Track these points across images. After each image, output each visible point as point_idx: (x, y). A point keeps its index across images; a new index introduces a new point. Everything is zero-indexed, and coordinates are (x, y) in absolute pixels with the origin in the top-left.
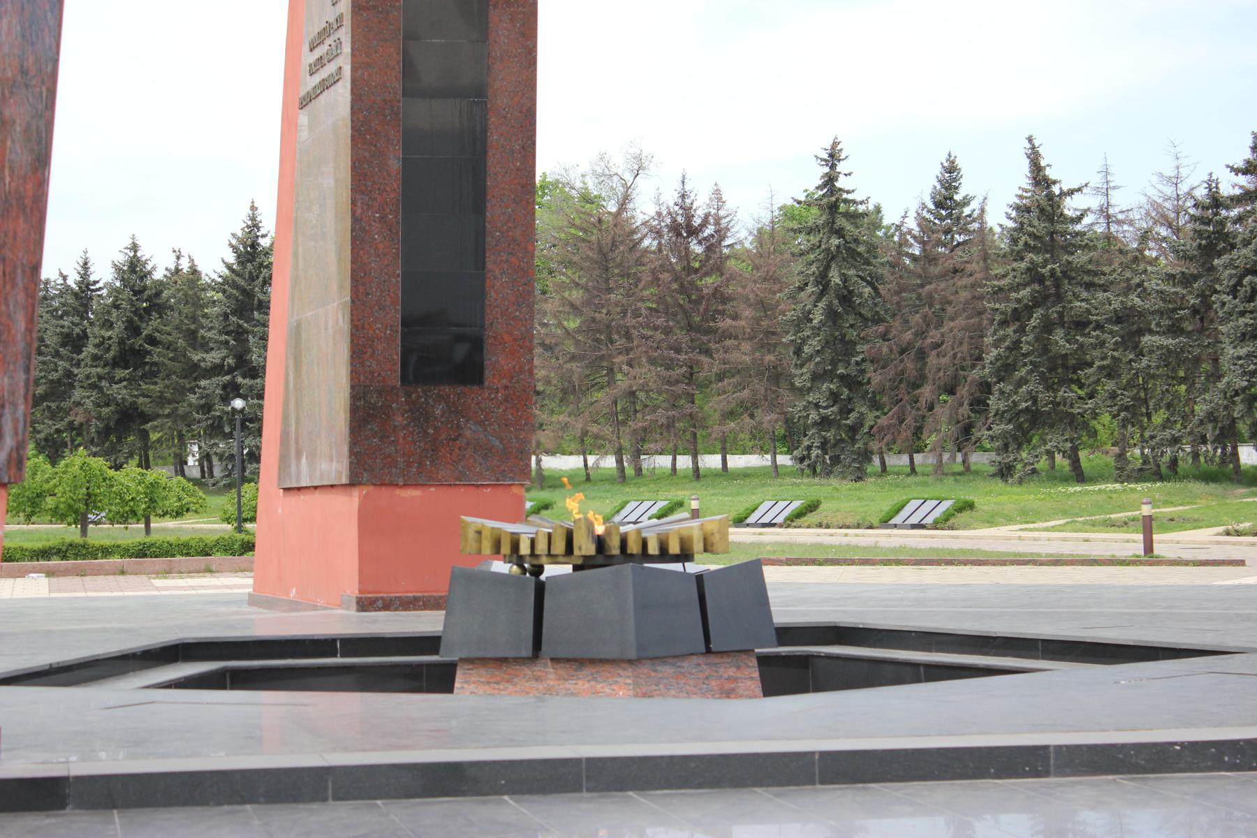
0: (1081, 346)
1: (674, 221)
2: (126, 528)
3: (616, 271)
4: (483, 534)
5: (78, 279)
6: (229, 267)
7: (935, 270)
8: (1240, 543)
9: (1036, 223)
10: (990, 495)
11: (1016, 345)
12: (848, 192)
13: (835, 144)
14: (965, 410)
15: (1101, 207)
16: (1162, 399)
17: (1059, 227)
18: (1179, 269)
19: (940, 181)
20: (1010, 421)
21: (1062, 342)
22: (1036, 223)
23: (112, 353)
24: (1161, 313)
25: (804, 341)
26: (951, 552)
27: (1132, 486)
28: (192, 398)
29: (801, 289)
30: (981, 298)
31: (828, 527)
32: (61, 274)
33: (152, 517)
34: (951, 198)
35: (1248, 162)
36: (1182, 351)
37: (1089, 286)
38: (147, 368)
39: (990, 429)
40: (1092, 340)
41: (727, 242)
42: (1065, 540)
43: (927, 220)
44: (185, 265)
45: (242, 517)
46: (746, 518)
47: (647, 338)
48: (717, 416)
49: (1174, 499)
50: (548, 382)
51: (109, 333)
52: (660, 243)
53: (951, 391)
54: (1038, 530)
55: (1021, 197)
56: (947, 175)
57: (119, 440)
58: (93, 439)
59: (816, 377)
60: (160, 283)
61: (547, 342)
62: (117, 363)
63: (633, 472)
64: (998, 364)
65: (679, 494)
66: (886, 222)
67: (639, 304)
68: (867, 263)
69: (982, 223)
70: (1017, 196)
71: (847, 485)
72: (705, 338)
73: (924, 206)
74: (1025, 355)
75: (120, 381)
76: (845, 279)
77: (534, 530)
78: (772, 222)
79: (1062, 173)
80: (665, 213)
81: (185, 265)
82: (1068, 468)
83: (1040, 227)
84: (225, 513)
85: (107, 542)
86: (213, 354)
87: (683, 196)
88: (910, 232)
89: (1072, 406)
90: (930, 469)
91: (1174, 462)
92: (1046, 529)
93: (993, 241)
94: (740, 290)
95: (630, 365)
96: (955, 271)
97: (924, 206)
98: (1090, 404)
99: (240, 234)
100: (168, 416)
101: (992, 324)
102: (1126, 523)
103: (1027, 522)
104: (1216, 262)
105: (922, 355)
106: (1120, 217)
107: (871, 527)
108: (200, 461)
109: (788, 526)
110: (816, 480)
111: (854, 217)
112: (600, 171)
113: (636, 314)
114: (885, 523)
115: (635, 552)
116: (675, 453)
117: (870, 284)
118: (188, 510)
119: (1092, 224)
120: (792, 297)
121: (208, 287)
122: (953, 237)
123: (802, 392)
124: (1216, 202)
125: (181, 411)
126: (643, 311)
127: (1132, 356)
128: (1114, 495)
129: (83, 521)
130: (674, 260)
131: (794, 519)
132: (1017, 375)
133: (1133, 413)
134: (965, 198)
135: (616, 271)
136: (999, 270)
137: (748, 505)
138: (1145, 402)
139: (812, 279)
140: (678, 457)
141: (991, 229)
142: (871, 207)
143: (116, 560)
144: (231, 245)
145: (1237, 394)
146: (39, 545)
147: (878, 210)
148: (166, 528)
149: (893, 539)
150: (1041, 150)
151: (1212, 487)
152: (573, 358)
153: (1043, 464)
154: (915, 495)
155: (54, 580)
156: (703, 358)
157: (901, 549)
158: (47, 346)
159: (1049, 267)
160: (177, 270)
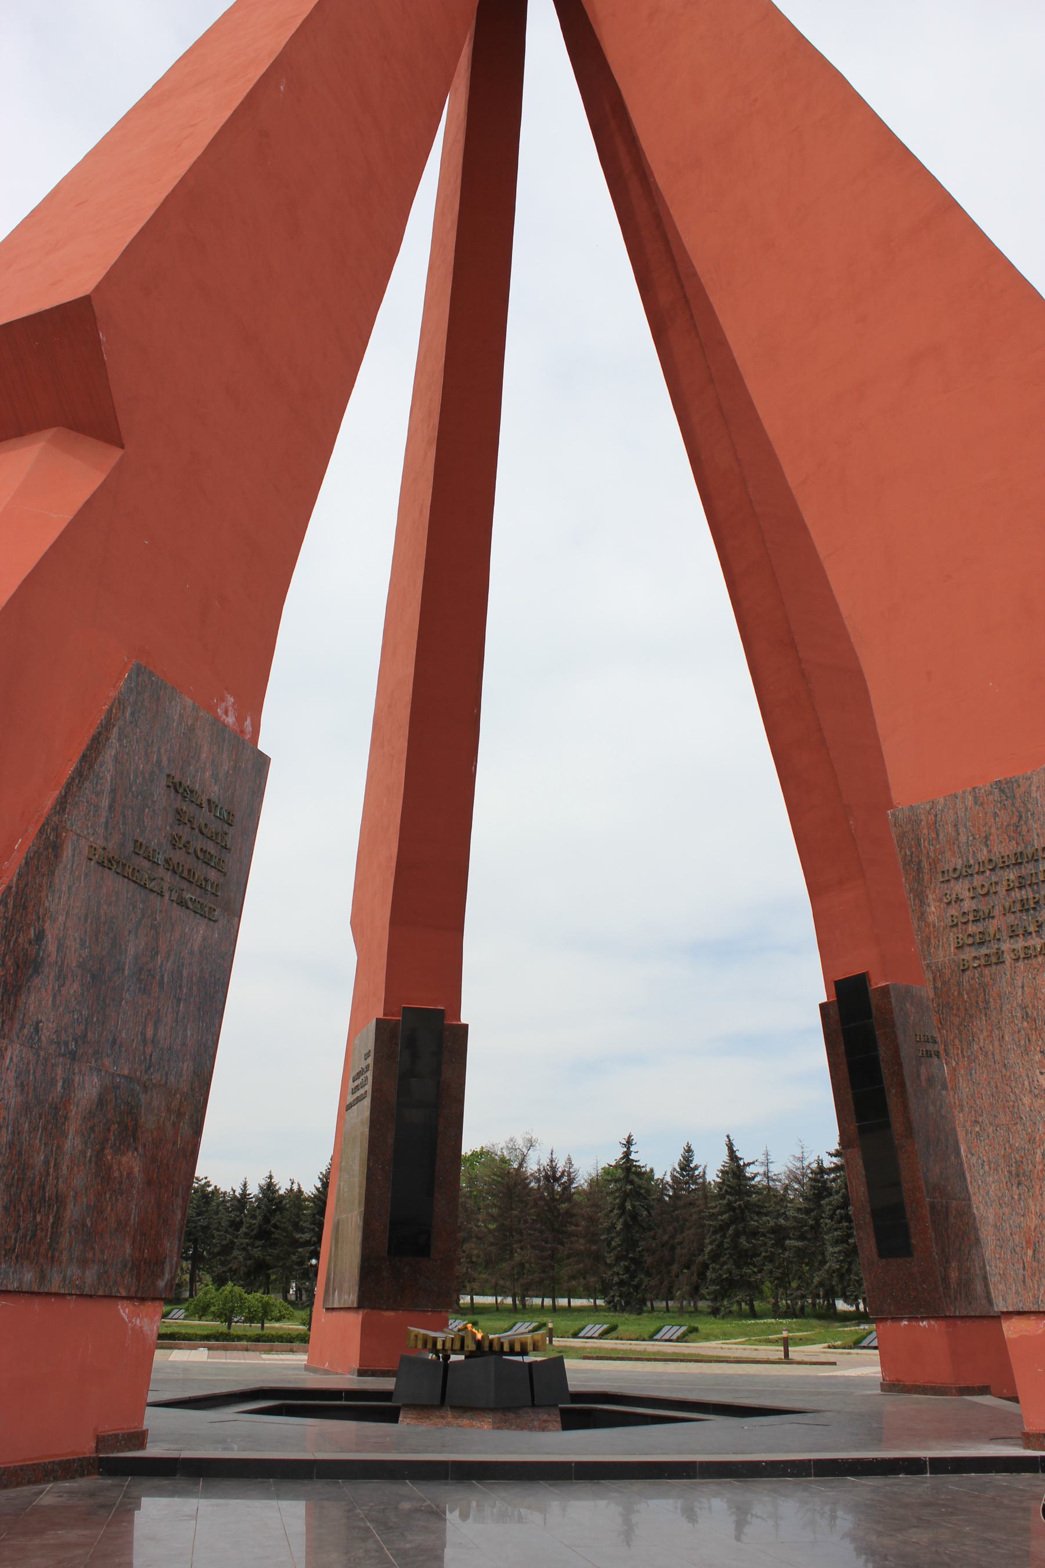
0: (755, 1245)
1: (546, 1173)
2: (251, 1326)
3: (516, 1199)
4: (419, 1337)
5: (241, 1192)
6: (317, 1189)
7: (680, 1203)
8: (836, 1353)
9: (731, 1180)
10: (705, 1325)
11: (721, 1244)
12: (636, 1161)
13: (630, 1137)
14: (695, 1278)
15: (765, 1172)
16: (796, 1275)
17: (743, 1182)
18: (804, 1205)
19: (683, 1157)
20: (717, 1285)
21: (745, 1243)
22: (731, 1180)
23: (255, 1232)
24: (794, 1228)
25: (612, 1239)
26: (684, 1355)
27: (781, 1320)
28: (294, 1258)
29: (611, 1211)
30: (703, 1218)
31: (621, 1339)
32: (232, 1189)
33: (265, 1320)
34: (689, 1166)
35: (837, 1150)
36: (806, 1249)
37: (759, 1214)
38: (272, 1241)
39: (707, 1288)
40: (759, 1242)
41: (574, 1186)
42: (745, 1349)
43: (675, 1176)
44: (295, 1188)
45: (308, 1322)
46: (579, 1333)
47: (531, 1235)
48: (566, 1278)
49: (802, 1328)
50: (478, 1256)
51: (255, 1221)
52: (539, 1185)
53: (688, 1268)
54: (731, 1344)
55: (724, 1166)
56: (686, 1154)
57: (255, 1278)
58: (241, 1277)
59: (618, 1259)
60: (282, 1196)
61: (479, 1235)
62: (258, 1237)
63: (521, 1307)
64: (712, 1253)
65: (544, 1319)
66: (656, 1177)
67: (527, 1217)
68: (645, 1198)
69: (705, 1179)
70: (722, 1165)
71: (633, 1317)
72: (561, 1236)
73: (675, 1169)
74: (726, 1249)
75: (257, 1247)
76: (633, 1206)
77: (444, 1335)
78: (597, 1175)
79: (745, 1154)
80: (542, 1170)
81: (295, 1188)
82: (748, 1311)
83: (733, 1182)
84: (303, 1320)
85: (240, 1333)
86: (307, 1235)
87: (552, 1161)
88: (667, 1183)
89: (750, 1277)
90: (676, 1309)
91: (802, 1308)
92: (736, 1343)
93: (711, 1189)
94: (580, 1211)
95: (522, 1248)
96: (690, 1204)
97: (675, 1169)
98: (759, 1276)
99: (324, 1172)
100: (281, 1266)
101: (709, 1232)
102: (777, 1341)
103: (726, 1339)
104: (822, 1202)
105: (673, 1248)
106: (774, 1177)
107: (644, 1340)
108: (296, 1291)
109: (601, 1339)
110: (617, 1314)
111: (640, 1175)
112: (510, 1146)
113: (526, 1222)
114: (651, 1338)
115: (497, 1350)
116: (543, 1297)
117: (647, 1210)
118: (284, 1318)
119: (760, 1181)
120: (607, 1216)
121: (306, 1199)
122: (689, 1186)
123: (610, 1266)
124: (821, 1170)
125: (288, 1264)
126: (529, 1220)
127: (781, 1251)
128: (771, 1326)
129: (229, 1321)
130: (546, 1194)
131: (603, 1335)
132: (722, 1259)
133: (782, 1282)
134: (696, 1166)
135: (516, 1199)
136: (713, 1204)
137: (580, 1326)
138: (788, 1275)
139: (616, 1206)
140: (545, 1299)
141: (710, 1182)
142: (648, 1170)
143: (245, 1343)
144: (319, 1178)
145: (834, 1272)
146: (205, 1333)
147: (652, 1170)
148: (273, 1326)
149: (655, 1347)
150: (733, 1142)
151: (822, 1322)
152: (492, 1244)
153: (735, 1308)
154: (668, 1323)
155: (211, 1352)
156: (559, 1246)
157: (658, 1353)
158: (222, 1227)
159: (738, 1203)
160: (291, 1190)
